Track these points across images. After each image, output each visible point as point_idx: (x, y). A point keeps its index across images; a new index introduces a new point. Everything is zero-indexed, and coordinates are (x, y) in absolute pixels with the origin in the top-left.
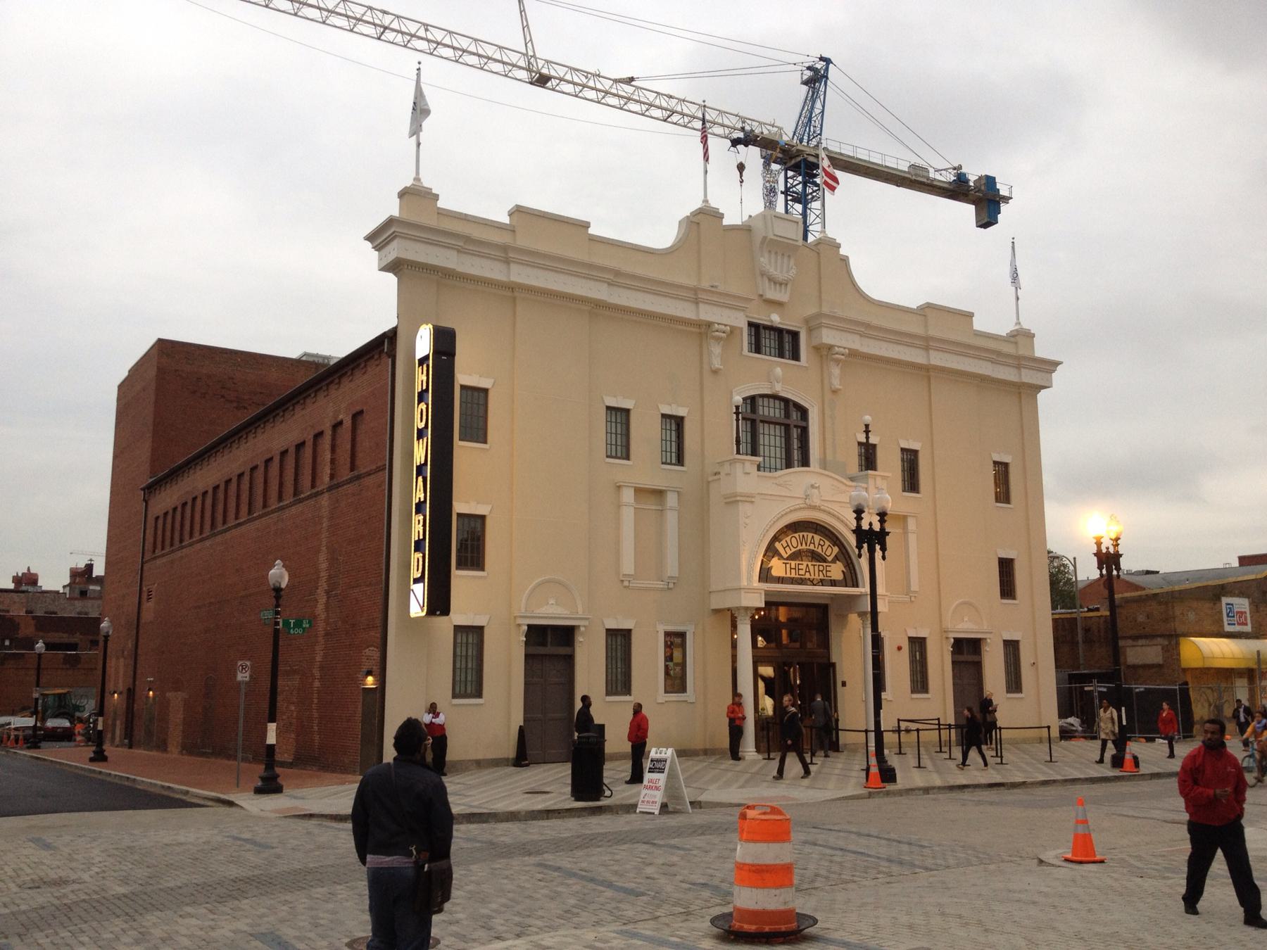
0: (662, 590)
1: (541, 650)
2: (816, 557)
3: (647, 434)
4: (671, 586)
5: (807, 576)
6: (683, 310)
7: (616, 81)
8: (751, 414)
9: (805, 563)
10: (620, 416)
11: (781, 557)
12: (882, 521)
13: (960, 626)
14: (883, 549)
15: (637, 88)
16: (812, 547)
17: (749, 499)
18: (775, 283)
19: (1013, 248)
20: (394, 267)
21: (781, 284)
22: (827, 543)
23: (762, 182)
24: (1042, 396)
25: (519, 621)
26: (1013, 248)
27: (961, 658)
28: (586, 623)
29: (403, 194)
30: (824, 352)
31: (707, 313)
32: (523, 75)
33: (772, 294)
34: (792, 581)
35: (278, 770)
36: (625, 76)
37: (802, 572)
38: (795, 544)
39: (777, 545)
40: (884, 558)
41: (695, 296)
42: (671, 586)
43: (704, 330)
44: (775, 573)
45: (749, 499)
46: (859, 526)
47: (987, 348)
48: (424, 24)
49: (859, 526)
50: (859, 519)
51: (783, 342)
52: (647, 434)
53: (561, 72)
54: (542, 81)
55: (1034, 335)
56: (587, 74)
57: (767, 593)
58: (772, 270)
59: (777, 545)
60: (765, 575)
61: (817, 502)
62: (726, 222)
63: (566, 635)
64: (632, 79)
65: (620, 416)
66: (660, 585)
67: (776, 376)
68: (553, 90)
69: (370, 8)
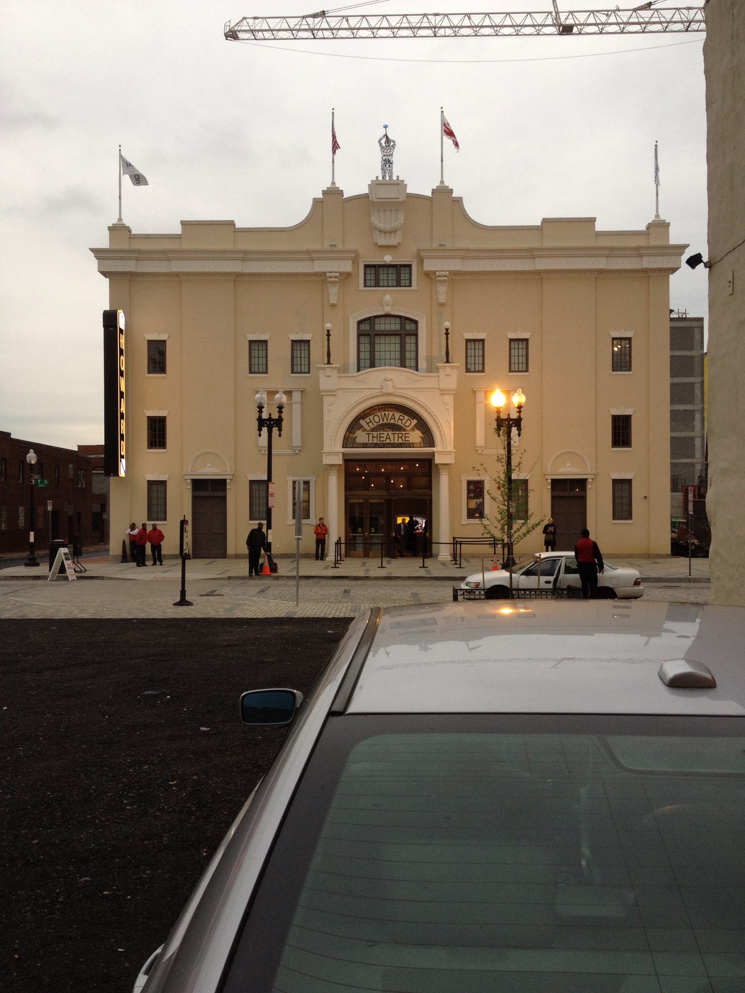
0: (291, 455)
1: (202, 494)
2: (395, 428)
3: (279, 355)
4: (297, 452)
5: (388, 441)
6: (304, 267)
7: (635, 10)
8: (369, 331)
9: (386, 433)
10: (258, 346)
11: (364, 430)
12: (280, 412)
13: (563, 470)
14: (280, 430)
15: (657, 10)
16: (393, 421)
17: (332, 393)
18: (385, 233)
19: (656, 150)
20: (105, 274)
21: (390, 233)
22: (406, 417)
23: (380, 155)
24: (673, 278)
25: (186, 477)
26: (656, 150)
27: (556, 494)
28: (231, 477)
29: (112, 229)
30: (429, 276)
31: (319, 267)
32: (553, 30)
33: (382, 241)
34: (376, 445)
35: (275, 561)
36: (643, 4)
37: (384, 439)
38: (397, 419)
39: (362, 422)
40: (280, 435)
41: (310, 256)
42: (297, 452)
43: (322, 278)
44: (358, 440)
45: (332, 393)
46: (260, 417)
47: (620, 244)
48: (466, 14)
49: (260, 417)
50: (260, 412)
51: (399, 274)
52: (279, 355)
53: (581, 18)
54: (567, 30)
55: (668, 225)
56: (608, 13)
57: (344, 454)
58: (381, 225)
59: (362, 422)
60: (348, 441)
61: (390, 390)
62: (346, 195)
63: (220, 485)
64: (650, 4)
65: (258, 346)
66: (289, 452)
67: (389, 301)
68: (580, 34)
69: (425, 15)
